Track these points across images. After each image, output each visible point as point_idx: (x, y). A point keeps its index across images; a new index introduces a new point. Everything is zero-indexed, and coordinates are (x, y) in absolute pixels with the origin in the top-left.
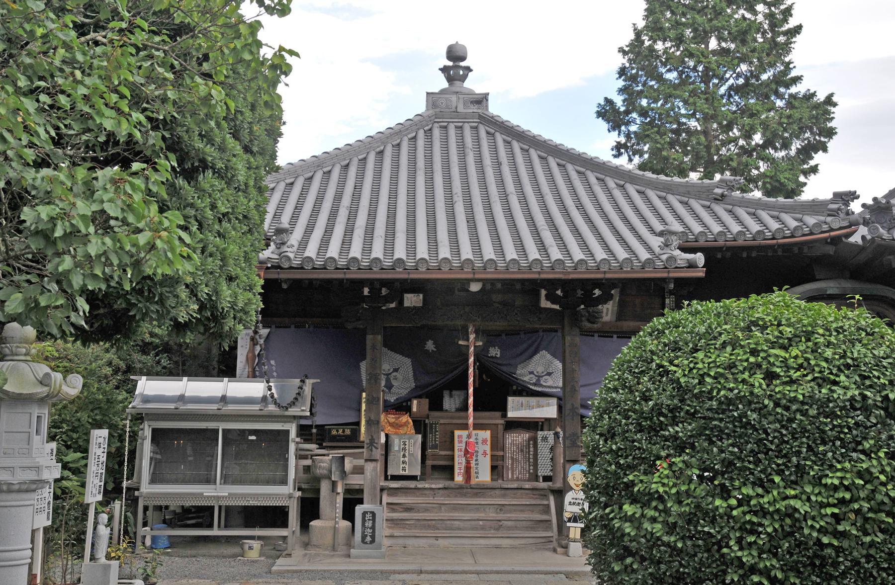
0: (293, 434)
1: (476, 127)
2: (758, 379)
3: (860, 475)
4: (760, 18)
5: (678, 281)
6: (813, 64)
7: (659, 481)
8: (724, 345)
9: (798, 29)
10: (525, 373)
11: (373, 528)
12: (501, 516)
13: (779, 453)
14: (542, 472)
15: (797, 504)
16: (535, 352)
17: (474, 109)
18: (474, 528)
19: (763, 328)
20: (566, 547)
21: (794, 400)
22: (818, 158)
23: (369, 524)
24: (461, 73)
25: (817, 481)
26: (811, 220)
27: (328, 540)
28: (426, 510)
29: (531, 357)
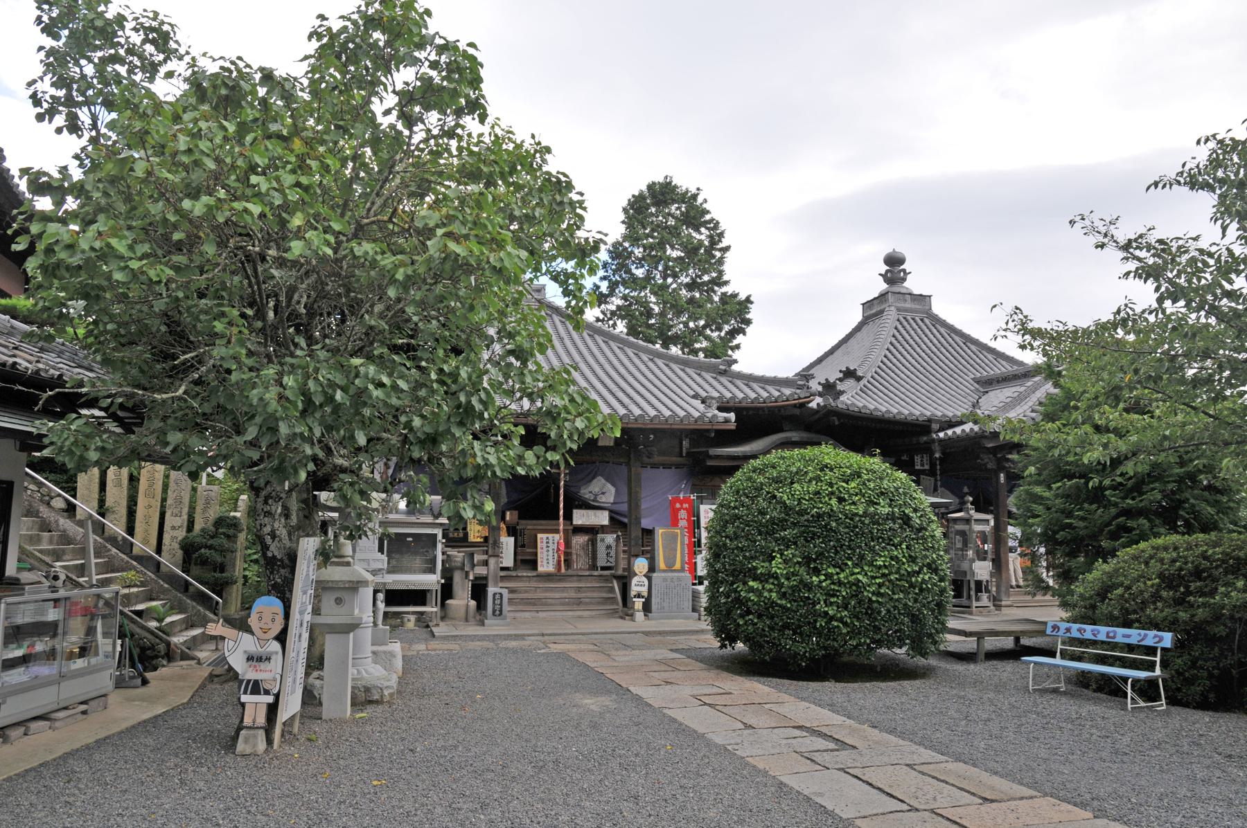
0: (440, 537)
2: (834, 501)
3: (892, 558)
4: (703, 237)
5: (717, 431)
6: (739, 276)
7: (777, 566)
8: (810, 481)
9: (727, 249)
10: (586, 492)
11: (501, 605)
12: (580, 595)
13: (849, 547)
14: (601, 562)
15: (860, 577)
16: (593, 478)
18: (563, 604)
19: (831, 470)
20: (632, 615)
21: (856, 514)
22: (740, 339)
23: (498, 602)
25: (871, 564)
26: (787, 391)
27: (462, 613)
28: (526, 592)
29: (590, 481)
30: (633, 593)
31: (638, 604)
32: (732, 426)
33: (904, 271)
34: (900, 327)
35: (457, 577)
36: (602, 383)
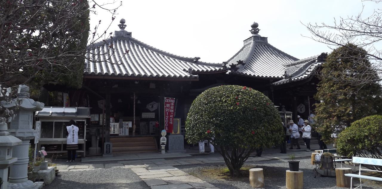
1: (128, 41)
10: (149, 107)
11: (109, 149)
17: (128, 36)
20: (160, 151)
24: (124, 26)
30: (161, 143)
31: (163, 147)
32: (198, 80)
33: (258, 29)
34: (255, 53)
35: (93, 138)
36: (150, 66)
